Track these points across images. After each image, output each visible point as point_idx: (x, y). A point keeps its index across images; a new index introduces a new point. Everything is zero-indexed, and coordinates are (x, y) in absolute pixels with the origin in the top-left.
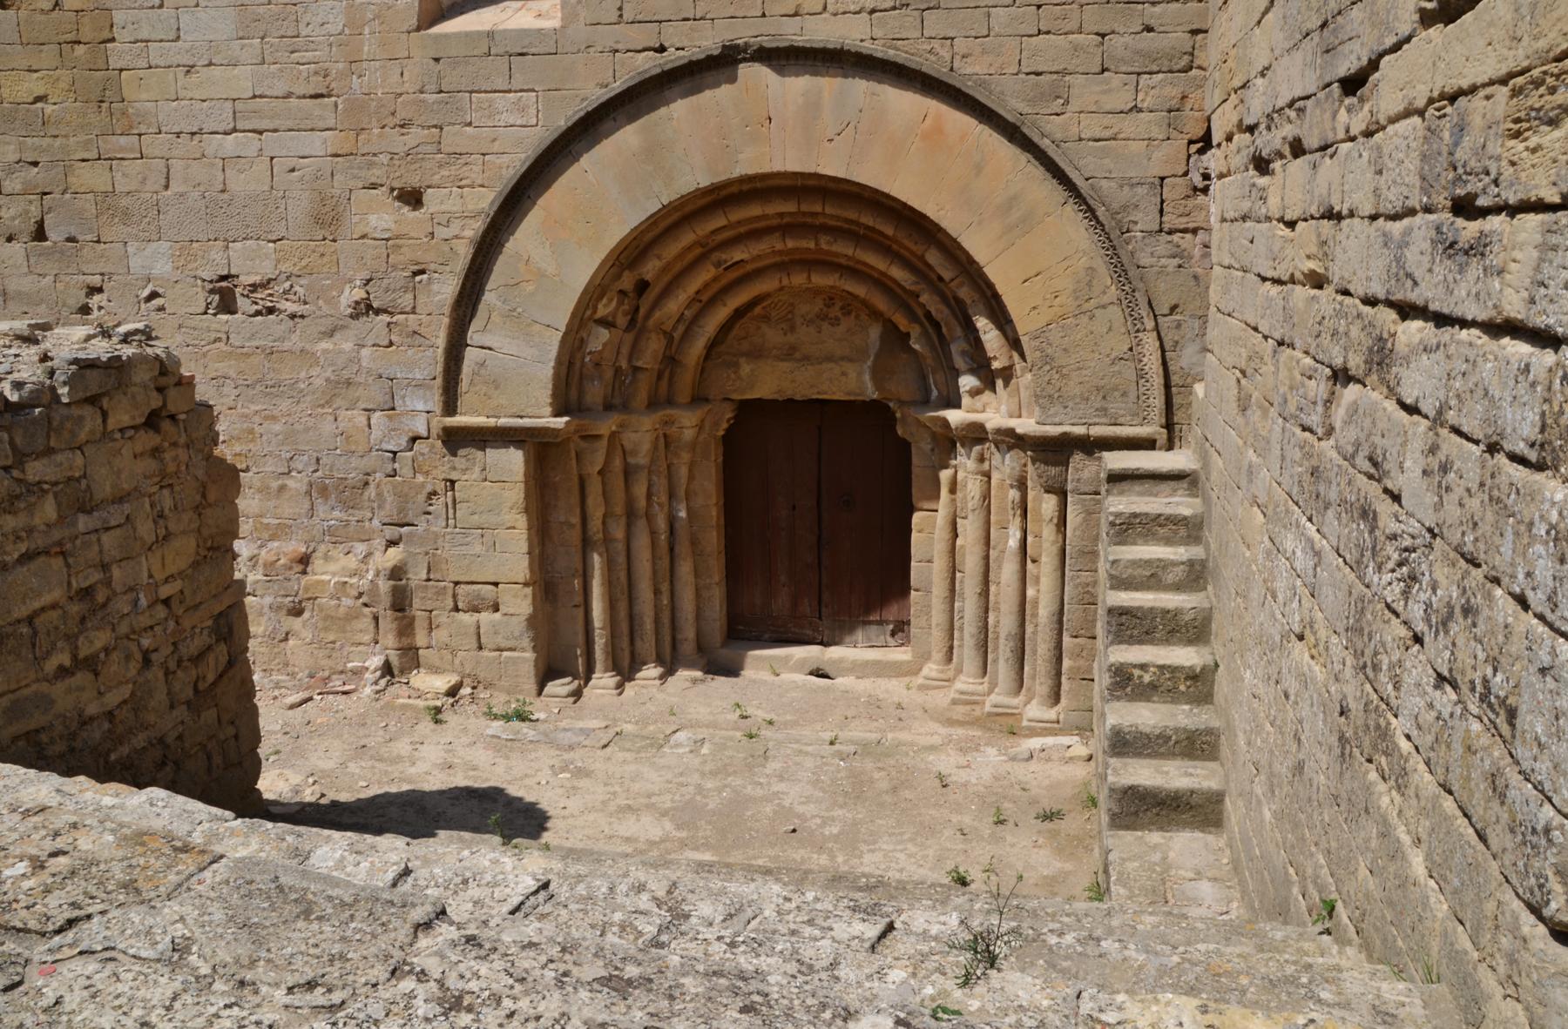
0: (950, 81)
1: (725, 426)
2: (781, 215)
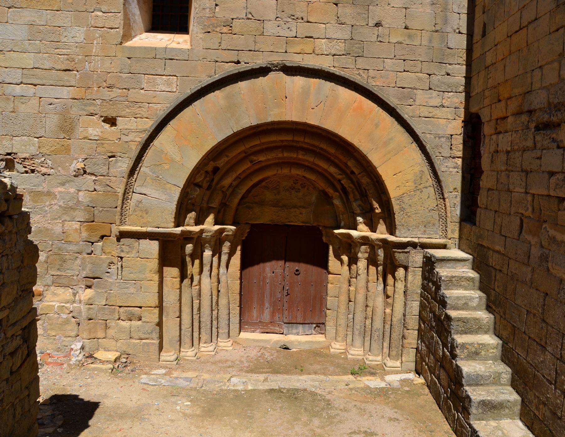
0: (367, 87)
1: (246, 235)
2: (282, 141)
